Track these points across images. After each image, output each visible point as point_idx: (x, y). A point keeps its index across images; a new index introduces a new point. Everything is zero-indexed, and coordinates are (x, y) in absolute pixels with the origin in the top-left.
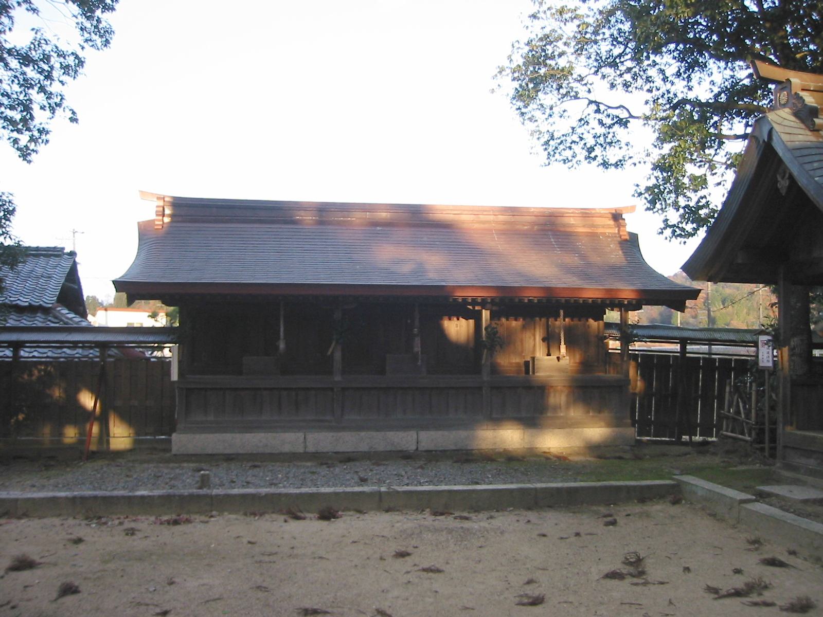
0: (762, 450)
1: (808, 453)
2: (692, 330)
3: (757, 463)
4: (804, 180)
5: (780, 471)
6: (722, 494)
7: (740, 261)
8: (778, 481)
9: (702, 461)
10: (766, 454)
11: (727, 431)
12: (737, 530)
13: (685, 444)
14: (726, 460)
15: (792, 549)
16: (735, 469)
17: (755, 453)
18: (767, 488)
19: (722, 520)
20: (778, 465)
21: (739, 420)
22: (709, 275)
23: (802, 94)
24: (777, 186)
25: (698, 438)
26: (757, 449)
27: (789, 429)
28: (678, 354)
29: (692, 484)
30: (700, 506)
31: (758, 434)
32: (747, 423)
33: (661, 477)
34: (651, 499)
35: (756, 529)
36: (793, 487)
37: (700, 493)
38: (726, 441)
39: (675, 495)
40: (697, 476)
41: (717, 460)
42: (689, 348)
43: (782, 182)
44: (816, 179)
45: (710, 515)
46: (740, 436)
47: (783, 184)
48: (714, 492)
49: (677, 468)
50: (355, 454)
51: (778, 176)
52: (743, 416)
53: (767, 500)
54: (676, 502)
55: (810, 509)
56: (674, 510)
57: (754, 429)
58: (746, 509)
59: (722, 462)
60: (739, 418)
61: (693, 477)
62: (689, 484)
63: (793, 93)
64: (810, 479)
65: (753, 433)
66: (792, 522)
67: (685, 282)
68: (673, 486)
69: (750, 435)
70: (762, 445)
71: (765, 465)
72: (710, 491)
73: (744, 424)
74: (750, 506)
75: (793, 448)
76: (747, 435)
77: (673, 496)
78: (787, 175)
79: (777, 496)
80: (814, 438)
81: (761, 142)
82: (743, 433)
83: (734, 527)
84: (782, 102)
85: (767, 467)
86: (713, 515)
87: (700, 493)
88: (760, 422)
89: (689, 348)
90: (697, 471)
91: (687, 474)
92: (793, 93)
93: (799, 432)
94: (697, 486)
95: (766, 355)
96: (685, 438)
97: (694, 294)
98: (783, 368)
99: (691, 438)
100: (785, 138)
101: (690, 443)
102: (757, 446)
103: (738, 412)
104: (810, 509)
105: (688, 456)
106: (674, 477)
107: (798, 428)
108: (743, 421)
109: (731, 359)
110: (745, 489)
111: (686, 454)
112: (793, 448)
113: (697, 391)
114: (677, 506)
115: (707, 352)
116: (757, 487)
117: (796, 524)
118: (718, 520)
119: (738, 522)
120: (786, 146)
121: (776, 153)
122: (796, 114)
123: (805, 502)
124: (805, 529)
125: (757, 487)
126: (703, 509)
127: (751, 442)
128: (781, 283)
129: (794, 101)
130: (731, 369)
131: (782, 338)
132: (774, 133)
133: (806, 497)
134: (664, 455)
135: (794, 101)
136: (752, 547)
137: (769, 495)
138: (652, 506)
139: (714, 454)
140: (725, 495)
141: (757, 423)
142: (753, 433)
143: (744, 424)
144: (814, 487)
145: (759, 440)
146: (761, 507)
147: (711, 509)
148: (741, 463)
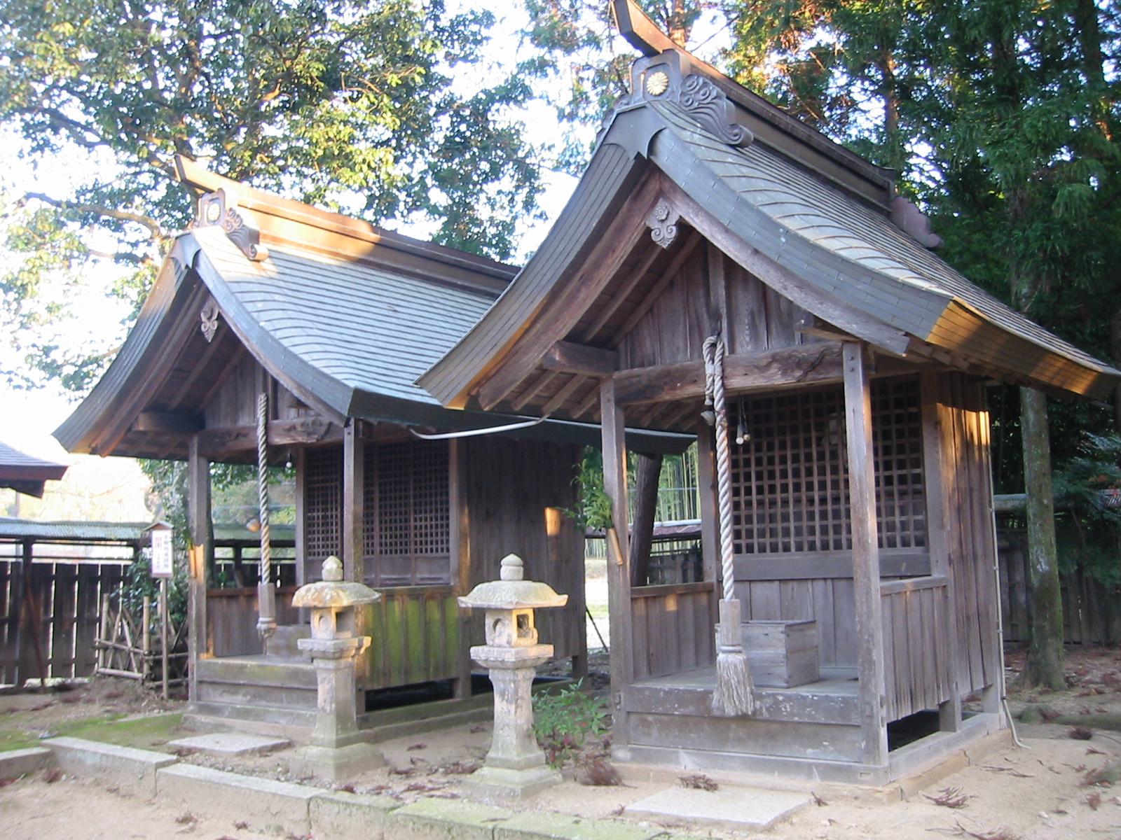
0: (159, 688)
1: (235, 687)
2: (38, 524)
3: (154, 709)
4: (243, 324)
5: (194, 716)
6: (127, 759)
7: (141, 428)
8: (193, 731)
9: (74, 713)
10: (164, 693)
11: (104, 666)
12: (155, 806)
13: (33, 691)
14: (109, 708)
15: (240, 821)
16: (125, 720)
17: (148, 694)
18: (185, 742)
19: (128, 796)
20: (191, 708)
21: (123, 650)
22: (93, 445)
23: (239, 211)
24: (200, 328)
25: (50, 682)
26: (152, 688)
27: (204, 657)
28: (231, 562)
29: (77, 750)
30: (91, 780)
31: (151, 668)
32: (135, 654)
33: (23, 744)
34: (12, 780)
35: (184, 801)
36: (218, 736)
37: (90, 761)
38: (103, 681)
39: (49, 768)
40: (74, 736)
41: (95, 710)
42: (38, 549)
43: (208, 324)
44: (262, 324)
45: (109, 790)
46: (126, 673)
47: (209, 328)
48: (114, 756)
49: (42, 728)
50: (389, 693)
51: (202, 314)
52: (130, 644)
53: (189, 758)
54: (53, 779)
55: (250, 763)
56: (54, 791)
57: (147, 661)
58: (166, 775)
59: (108, 711)
60: (124, 647)
61: (75, 739)
62: (72, 749)
63: (227, 207)
64: (238, 723)
65: (146, 667)
66: (237, 784)
67: (53, 454)
68: (44, 756)
69: (140, 670)
70: (158, 683)
71: (166, 710)
72: (107, 756)
73: (132, 655)
74: (170, 770)
75: (213, 683)
76: (136, 670)
77: (44, 771)
78: (215, 317)
79: (201, 751)
80: (242, 667)
81: (183, 267)
82: (129, 668)
83: (150, 803)
84: (212, 218)
85: (169, 713)
86: (114, 791)
87: (90, 761)
88: (155, 650)
89: (38, 549)
90: (74, 729)
91: (60, 735)
92: (227, 207)
93: (220, 661)
94: (84, 751)
95: (162, 558)
96: (34, 682)
97: (57, 472)
98: (196, 574)
99: (42, 681)
100: (220, 267)
101: (42, 690)
102: (152, 684)
103: (122, 639)
104: (250, 763)
105: (50, 708)
106: (45, 741)
107: (216, 655)
108: (130, 652)
109: (97, 566)
110: (155, 746)
111: (46, 706)
112: (213, 683)
113: (47, 612)
114: (54, 785)
115: (14, 554)
116: (171, 743)
117: (243, 786)
118: (124, 796)
119: (156, 795)
120: (219, 277)
121: (201, 282)
122: (231, 236)
123: (242, 754)
124: (258, 791)
125: (171, 743)
126: (97, 783)
127: (143, 680)
128: (194, 458)
129: (228, 218)
130: (97, 579)
131: (195, 534)
132: (201, 256)
133: (243, 748)
134: (13, 711)
135: (228, 218)
136: (185, 827)
137: (190, 751)
138: (17, 789)
139: (90, 701)
140: (132, 760)
141: (150, 653)
142: (146, 667)
143: (132, 655)
144: (244, 732)
145: (155, 676)
146: (184, 769)
147: (108, 781)
148: (133, 711)
